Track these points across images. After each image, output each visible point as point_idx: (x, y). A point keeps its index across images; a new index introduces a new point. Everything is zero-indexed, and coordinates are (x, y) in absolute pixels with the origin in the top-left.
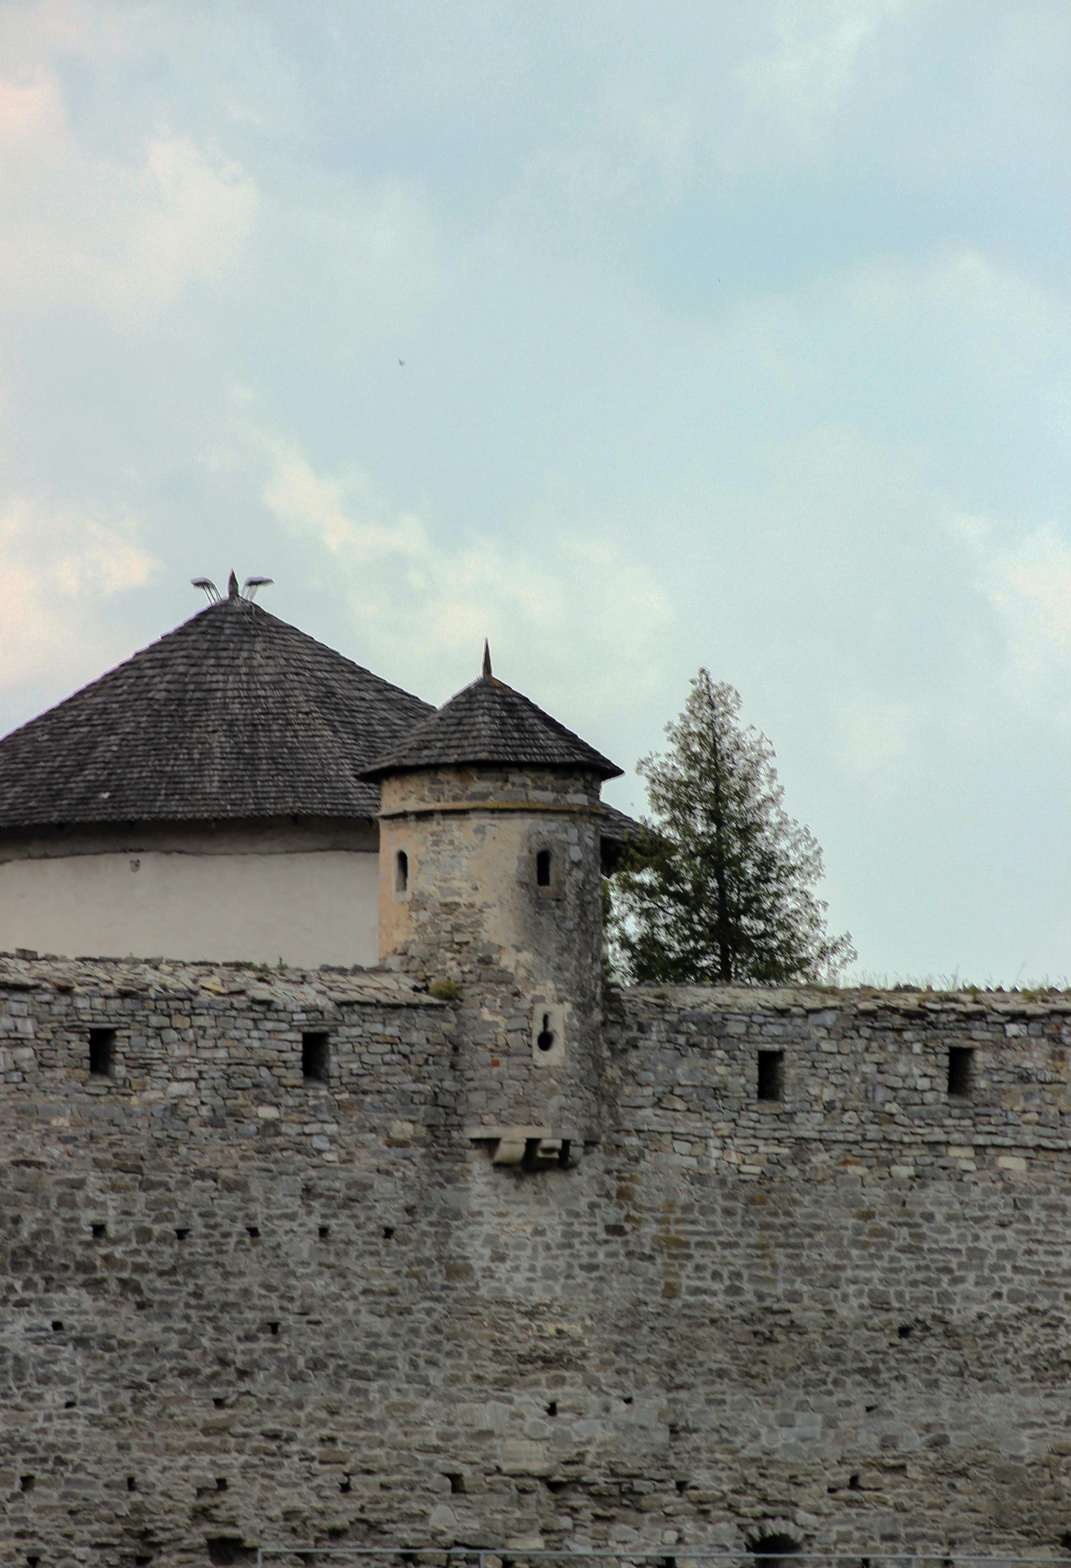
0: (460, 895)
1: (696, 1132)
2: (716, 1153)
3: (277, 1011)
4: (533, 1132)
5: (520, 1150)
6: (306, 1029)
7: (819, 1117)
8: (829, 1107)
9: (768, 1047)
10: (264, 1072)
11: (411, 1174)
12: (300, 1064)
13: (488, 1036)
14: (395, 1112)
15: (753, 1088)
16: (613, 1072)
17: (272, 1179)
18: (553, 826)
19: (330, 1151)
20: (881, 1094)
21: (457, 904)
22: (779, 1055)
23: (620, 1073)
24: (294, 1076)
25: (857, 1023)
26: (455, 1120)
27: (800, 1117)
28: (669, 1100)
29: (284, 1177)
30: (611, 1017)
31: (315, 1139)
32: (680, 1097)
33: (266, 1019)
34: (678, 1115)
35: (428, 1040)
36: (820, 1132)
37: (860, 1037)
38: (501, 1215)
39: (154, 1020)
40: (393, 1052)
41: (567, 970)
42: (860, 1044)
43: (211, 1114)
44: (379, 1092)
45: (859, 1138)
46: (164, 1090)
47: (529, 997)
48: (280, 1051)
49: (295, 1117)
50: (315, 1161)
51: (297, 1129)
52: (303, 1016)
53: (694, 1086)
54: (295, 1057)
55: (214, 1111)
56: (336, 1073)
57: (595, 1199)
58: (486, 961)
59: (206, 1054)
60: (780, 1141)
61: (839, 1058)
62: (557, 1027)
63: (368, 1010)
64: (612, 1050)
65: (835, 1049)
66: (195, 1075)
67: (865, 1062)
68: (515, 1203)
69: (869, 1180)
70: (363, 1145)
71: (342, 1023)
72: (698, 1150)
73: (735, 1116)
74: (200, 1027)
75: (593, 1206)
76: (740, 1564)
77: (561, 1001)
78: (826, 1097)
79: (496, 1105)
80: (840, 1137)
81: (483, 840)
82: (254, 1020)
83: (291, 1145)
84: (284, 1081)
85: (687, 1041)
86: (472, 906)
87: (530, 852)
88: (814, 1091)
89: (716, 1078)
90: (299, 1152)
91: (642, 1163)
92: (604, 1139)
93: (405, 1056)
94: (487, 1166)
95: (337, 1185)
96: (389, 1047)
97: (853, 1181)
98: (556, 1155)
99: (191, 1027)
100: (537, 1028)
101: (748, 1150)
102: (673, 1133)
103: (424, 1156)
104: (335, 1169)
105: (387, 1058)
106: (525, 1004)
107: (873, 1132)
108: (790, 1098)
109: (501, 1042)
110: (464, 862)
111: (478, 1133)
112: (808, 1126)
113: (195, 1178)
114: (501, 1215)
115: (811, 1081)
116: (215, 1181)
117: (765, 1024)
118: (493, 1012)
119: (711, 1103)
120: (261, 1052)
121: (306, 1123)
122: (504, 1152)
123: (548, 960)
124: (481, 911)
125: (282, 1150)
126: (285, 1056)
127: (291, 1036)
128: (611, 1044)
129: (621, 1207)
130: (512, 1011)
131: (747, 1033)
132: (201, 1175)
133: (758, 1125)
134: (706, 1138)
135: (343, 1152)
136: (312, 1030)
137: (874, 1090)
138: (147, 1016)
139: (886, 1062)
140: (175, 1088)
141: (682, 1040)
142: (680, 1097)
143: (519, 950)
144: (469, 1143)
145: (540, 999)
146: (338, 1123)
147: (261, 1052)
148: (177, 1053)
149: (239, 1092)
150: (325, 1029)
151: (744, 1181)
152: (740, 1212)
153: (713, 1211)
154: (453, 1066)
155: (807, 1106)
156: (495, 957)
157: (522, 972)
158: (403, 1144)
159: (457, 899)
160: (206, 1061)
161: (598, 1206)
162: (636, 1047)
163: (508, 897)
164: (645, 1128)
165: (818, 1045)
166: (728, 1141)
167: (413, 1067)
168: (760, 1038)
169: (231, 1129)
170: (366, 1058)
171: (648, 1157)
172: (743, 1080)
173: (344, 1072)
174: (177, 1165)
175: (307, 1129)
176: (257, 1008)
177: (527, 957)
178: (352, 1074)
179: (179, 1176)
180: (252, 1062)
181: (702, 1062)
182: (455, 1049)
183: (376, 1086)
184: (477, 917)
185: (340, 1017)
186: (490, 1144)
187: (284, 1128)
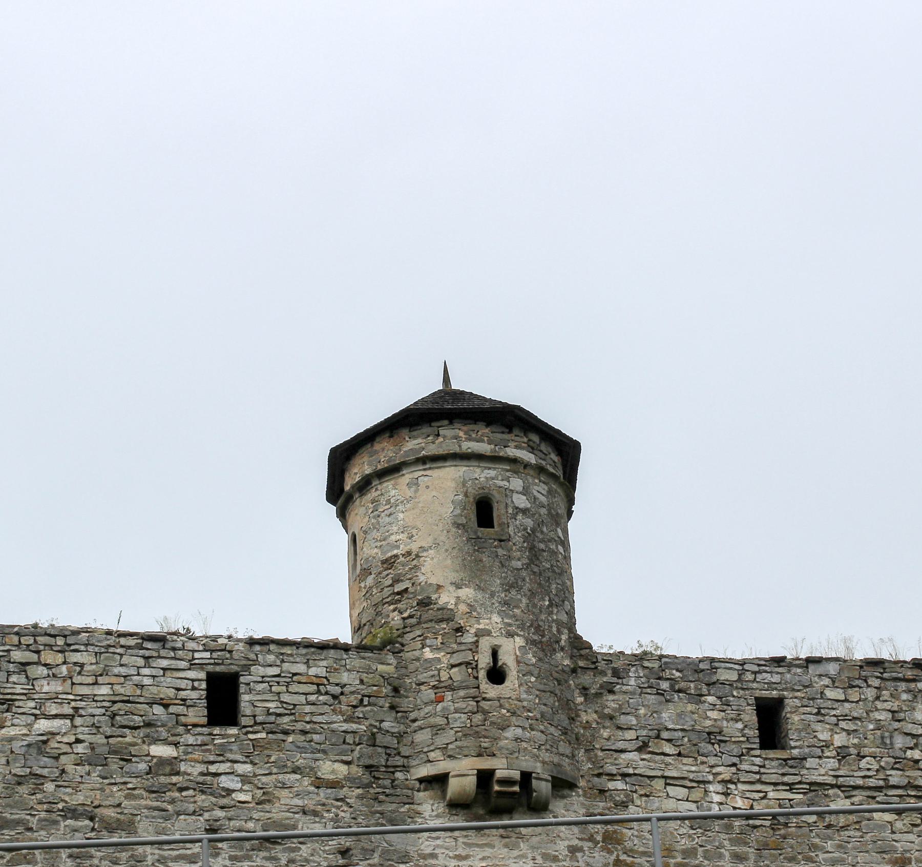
0: (398, 547)
1: (691, 776)
2: (717, 798)
3: (174, 649)
4: (486, 764)
5: (470, 783)
6: (210, 668)
7: (833, 763)
8: (842, 754)
9: (765, 694)
10: (158, 710)
11: (345, 815)
12: (204, 703)
13: (432, 673)
14: (324, 752)
15: (754, 733)
16: (588, 716)
17: (166, 819)
18: (492, 473)
19: (241, 790)
20: (900, 741)
21: (396, 556)
22: (779, 703)
23: (595, 716)
24: (197, 714)
25: (864, 674)
26: (399, 761)
27: (811, 763)
28: (656, 744)
29: (182, 817)
30: (581, 663)
31: (223, 778)
32: (669, 741)
33: (159, 657)
34: (668, 759)
35: (362, 682)
36: (837, 777)
37: (869, 686)
38: (459, 857)
39: (17, 655)
40: (319, 692)
41: (517, 607)
42: (870, 693)
43: (88, 751)
44: (304, 732)
45: (881, 783)
46: (29, 726)
47: (473, 631)
48: (178, 689)
49: (197, 755)
50: (225, 801)
51: (201, 768)
52: (207, 655)
53: (682, 730)
54: (198, 695)
55: (93, 749)
56: (248, 712)
57: (575, 842)
58: (425, 603)
59: (85, 690)
60: (791, 787)
61: (847, 705)
62: (507, 658)
63: (288, 650)
64: (585, 696)
65: (842, 697)
66: (71, 711)
67: (877, 710)
68: (478, 845)
69: (899, 825)
70: (284, 786)
71: (256, 662)
72: (697, 794)
73: (736, 760)
74: (75, 664)
75: (573, 850)
76: (325, 864)
77: (510, 635)
78: (837, 743)
79: (441, 740)
80: (860, 782)
81: (416, 491)
82: (146, 658)
83: (192, 785)
84: (183, 719)
85: (672, 687)
86: (409, 553)
87: (466, 495)
88: (824, 736)
89: (708, 723)
90: (203, 792)
91: (632, 808)
92: (582, 783)
93: (335, 697)
94: (441, 808)
95: (251, 825)
96: (315, 687)
97: (881, 827)
98: (516, 788)
99: (64, 663)
100: (484, 660)
101: (757, 796)
102: (666, 778)
103: (360, 797)
104: (249, 809)
105: (312, 698)
106: (469, 638)
107: (896, 778)
108: (796, 744)
109: (444, 676)
110: (401, 516)
111: (425, 771)
112: (821, 770)
113: (65, 817)
114: (459, 857)
115: (818, 727)
116: (92, 819)
117: (759, 672)
118: (434, 649)
119: (706, 747)
120: (154, 690)
121: (213, 763)
122: (454, 786)
123: (492, 595)
124: (417, 556)
125: (181, 790)
126: (183, 694)
127: (192, 674)
128: (584, 690)
129: (610, 852)
130: (455, 646)
131: (740, 680)
132: (72, 813)
133: (762, 770)
134: (704, 782)
135: (259, 793)
136: (218, 669)
137: (891, 737)
138: (8, 651)
139: (901, 710)
140: (43, 725)
141: (665, 685)
142: (669, 741)
143: (458, 587)
144: (417, 785)
145: (488, 633)
146: (252, 763)
147: (154, 690)
148: (46, 689)
149: (127, 731)
150: (234, 668)
151: (755, 827)
152: (752, 857)
153: (721, 856)
154: (392, 707)
155: (818, 752)
156: (434, 597)
157: (463, 608)
158: (334, 785)
159: (395, 552)
160: (83, 698)
161: (581, 849)
162: (611, 692)
163: (443, 538)
164: (631, 771)
165: (822, 693)
166: (732, 786)
167: (344, 708)
168: (755, 685)
169: (114, 767)
170: (286, 698)
171: (638, 802)
172: (740, 725)
173: (258, 711)
174: (40, 803)
175: (213, 769)
176: (149, 645)
177: (467, 593)
178: (269, 714)
179: (43, 815)
180: (142, 700)
181: (690, 707)
182: (396, 690)
183: (299, 726)
184: (415, 562)
185: (252, 656)
186: (439, 781)
187: (183, 767)
